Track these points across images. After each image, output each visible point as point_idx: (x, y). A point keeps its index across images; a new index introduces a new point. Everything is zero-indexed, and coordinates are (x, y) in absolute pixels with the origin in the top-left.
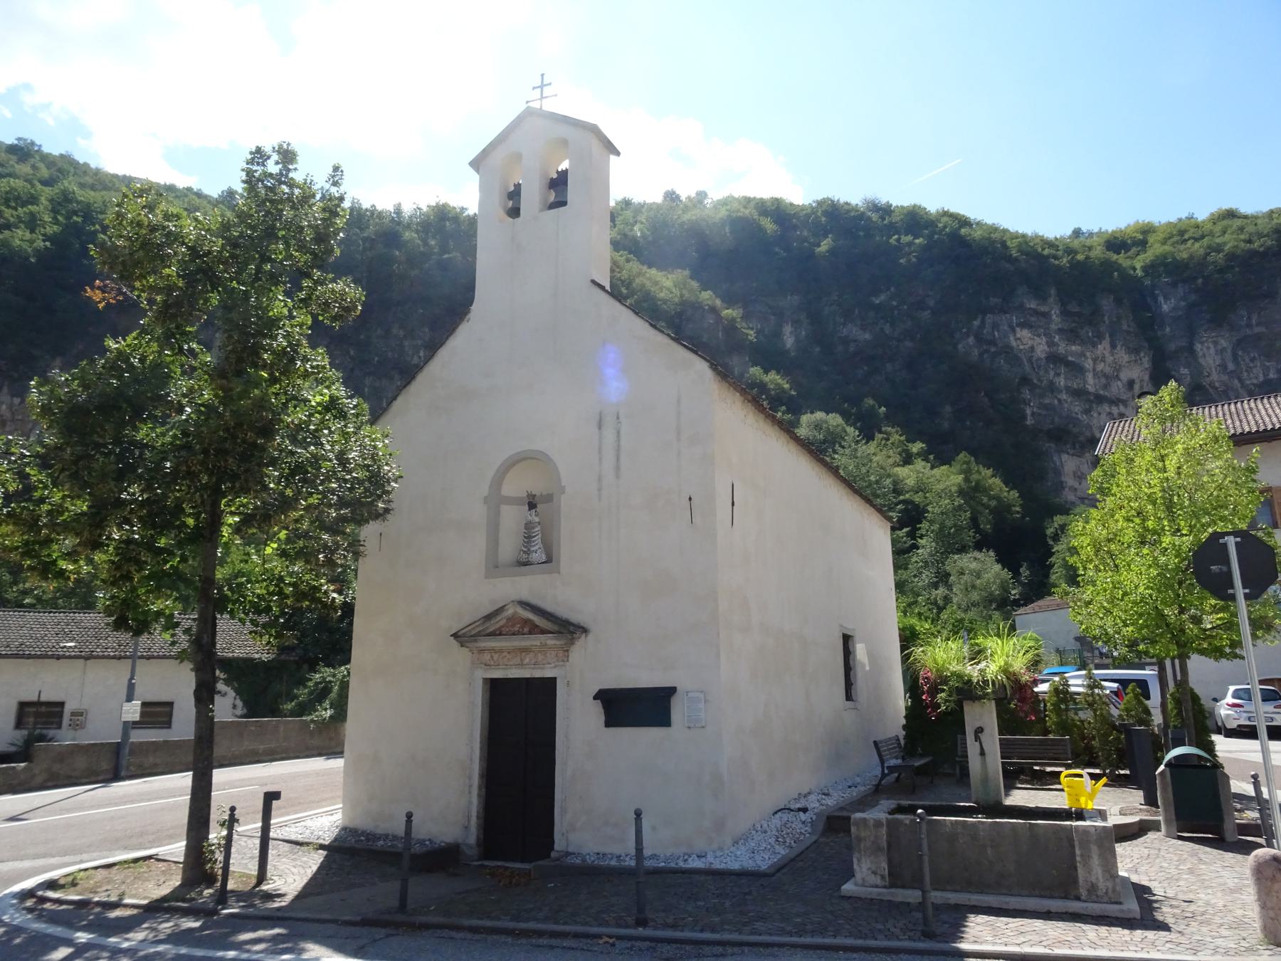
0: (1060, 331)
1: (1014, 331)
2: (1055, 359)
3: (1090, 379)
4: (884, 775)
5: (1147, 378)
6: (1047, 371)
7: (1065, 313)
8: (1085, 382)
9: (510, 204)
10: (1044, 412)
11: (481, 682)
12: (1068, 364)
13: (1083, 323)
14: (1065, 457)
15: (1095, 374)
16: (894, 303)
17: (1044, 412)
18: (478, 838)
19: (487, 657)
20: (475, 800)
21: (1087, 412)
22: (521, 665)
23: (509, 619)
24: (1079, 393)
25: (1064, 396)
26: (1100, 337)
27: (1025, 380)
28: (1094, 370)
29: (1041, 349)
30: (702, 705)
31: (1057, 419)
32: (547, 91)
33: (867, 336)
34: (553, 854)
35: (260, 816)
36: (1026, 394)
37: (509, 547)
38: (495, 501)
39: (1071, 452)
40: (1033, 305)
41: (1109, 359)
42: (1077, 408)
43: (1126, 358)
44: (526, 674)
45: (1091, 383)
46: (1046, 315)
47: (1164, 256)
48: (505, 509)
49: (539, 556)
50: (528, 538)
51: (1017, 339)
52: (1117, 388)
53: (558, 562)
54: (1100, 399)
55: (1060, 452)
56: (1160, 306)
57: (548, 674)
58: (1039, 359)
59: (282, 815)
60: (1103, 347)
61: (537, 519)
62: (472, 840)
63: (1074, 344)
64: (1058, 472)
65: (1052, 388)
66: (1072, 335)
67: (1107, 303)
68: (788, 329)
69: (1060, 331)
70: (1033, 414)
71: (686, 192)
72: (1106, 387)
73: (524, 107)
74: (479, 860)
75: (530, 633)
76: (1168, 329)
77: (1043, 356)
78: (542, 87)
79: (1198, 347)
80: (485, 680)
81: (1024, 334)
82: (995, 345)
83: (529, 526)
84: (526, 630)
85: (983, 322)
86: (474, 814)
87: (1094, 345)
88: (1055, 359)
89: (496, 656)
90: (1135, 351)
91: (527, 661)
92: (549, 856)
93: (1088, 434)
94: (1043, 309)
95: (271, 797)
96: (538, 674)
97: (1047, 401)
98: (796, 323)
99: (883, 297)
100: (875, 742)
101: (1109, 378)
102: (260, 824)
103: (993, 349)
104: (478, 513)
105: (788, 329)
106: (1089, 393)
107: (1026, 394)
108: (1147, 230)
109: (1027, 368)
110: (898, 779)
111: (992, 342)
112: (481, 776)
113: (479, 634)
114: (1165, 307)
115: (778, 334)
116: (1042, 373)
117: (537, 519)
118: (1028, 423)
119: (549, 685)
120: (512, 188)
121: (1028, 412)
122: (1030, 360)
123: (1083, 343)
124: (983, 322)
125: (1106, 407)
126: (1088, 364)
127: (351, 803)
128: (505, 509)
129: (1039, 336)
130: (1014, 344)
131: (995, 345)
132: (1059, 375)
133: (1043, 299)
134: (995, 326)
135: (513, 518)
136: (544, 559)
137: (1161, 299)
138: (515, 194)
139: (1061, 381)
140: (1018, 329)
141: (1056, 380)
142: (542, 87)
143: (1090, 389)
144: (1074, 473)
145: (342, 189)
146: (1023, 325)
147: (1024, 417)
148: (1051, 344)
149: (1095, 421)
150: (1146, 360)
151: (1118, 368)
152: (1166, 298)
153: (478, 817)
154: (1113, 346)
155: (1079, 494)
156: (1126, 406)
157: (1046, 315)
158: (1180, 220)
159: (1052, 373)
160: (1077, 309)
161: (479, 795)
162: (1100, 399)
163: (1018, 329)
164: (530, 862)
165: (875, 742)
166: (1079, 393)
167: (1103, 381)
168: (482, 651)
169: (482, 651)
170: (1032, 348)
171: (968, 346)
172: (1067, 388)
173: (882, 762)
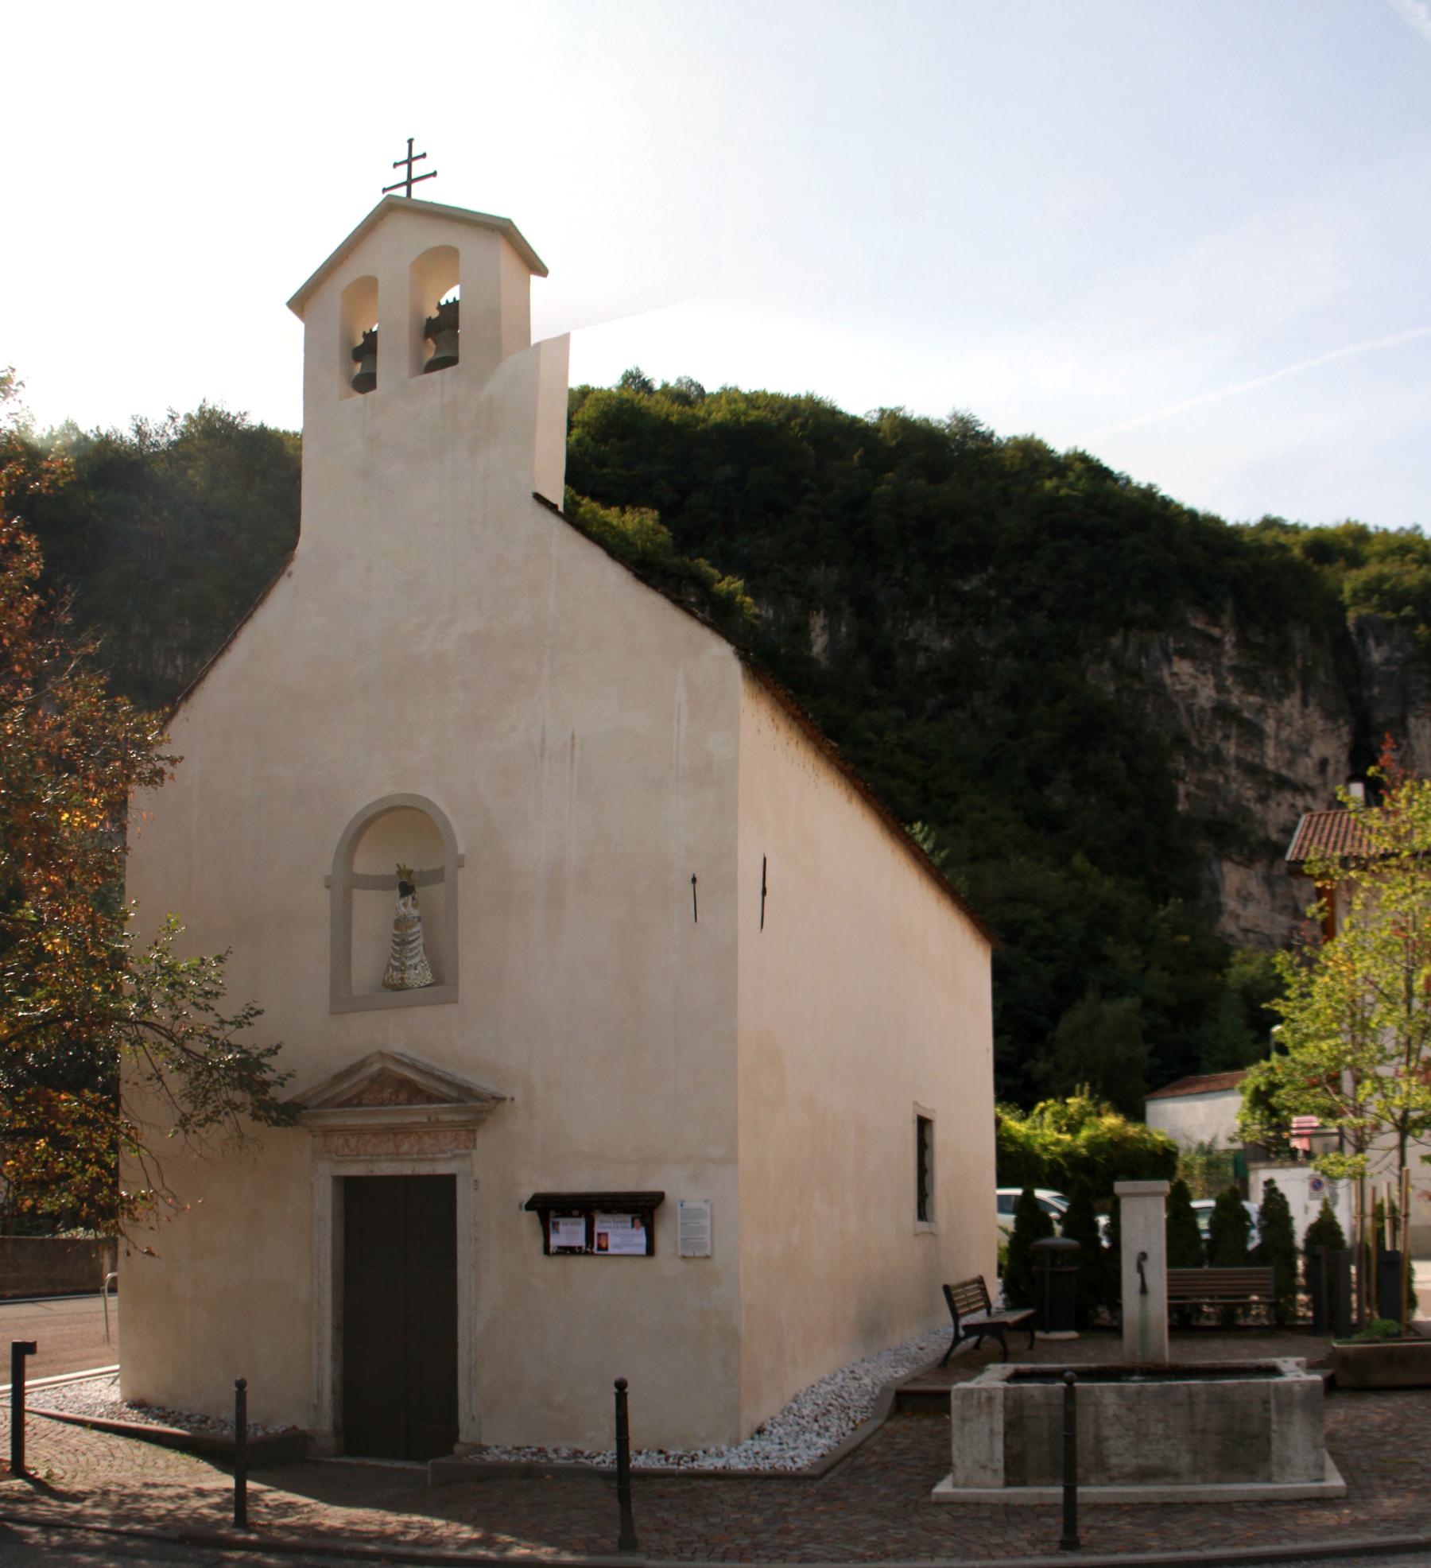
0: (1235, 670)
1: (1170, 661)
2: (1224, 713)
3: (1271, 751)
4: (957, 1339)
5: (1344, 758)
6: (1211, 731)
7: (1243, 643)
8: (1263, 754)
9: (358, 368)
10: (1202, 794)
11: (329, 1182)
12: (1243, 723)
13: (1265, 667)
14: (1227, 867)
15: (1278, 743)
16: (992, 593)
17: (1202, 794)
18: (335, 1425)
19: (338, 1141)
20: (328, 1367)
21: (1262, 799)
22: (397, 1156)
23: (372, 1079)
24: (1253, 771)
25: (1233, 771)
26: (1287, 688)
27: (1181, 741)
28: (1277, 735)
29: (1207, 695)
30: (706, 1222)
31: (1220, 807)
32: (419, 168)
33: (946, 643)
34: (457, 1448)
35: (8, 1374)
36: (1180, 763)
37: (368, 962)
38: (346, 885)
39: (1237, 858)
40: (1199, 625)
41: (1299, 729)
42: (1248, 792)
43: (1320, 724)
44: (406, 1169)
45: (1272, 756)
46: (1217, 642)
47: (1381, 579)
48: (359, 895)
49: (419, 974)
50: (402, 943)
51: (1174, 675)
52: (1305, 769)
53: (456, 984)
54: (1282, 783)
55: (1222, 855)
56: (1368, 654)
57: (442, 1169)
58: (1202, 709)
59: (36, 1377)
60: (1291, 705)
61: (416, 913)
62: (326, 1426)
63: (1252, 693)
64: (1216, 888)
65: (1218, 757)
66: (1250, 680)
67: (1299, 637)
68: (818, 622)
69: (1235, 670)
70: (1188, 795)
71: (662, 374)
72: (1290, 763)
73: (381, 197)
74: (336, 1455)
75: (410, 1102)
76: (1376, 690)
77: (1208, 705)
78: (409, 161)
79: (1412, 722)
80: (337, 1179)
81: (1183, 667)
82: (1141, 679)
83: (401, 923)
84: (402, 1097)
85: (1126, 641)
86: (327, 1386)
87: (1280, 698)
88: (1224, 713)
89: (353, 1142)
90: (1329, 715)
91: (405, 1148)
92: (451, 1452)
93: (1261, 834)
94: (1216, 632)
95: (22, 1351)
96: (424, 1169)
97: (1209, 777)
98: (833, 613)
99: (975, 581)
100: (947, 1289)
101: (1298, 750)
102: (9, 1386)
103: (1137, 686)
104: (321, 900)
105: (818, 622)
106: (1266, 771)
107: (1180, 763)
108: (1359, 535)
109: (1185, 723)
110: (977, 1346)
111: (1137, 674)
112: (336, 1329)
113: (325, 1104)
114: (1376, 656)
115: (800, 630)
116: (1204, 732)
117: (416, 913)
118: (1180, 808)
119: (450, 1181)
120: (360, 341)
121: (1182, 789)
122: (1189, 711)
123: (1264, 692)
124: (1126, 641)
125: (1288, 796)
126: (1270, 726)
127: (133, 1365)
128: (359, 895)
129: (1204, 673)
130: (1168, 681)
131: (1141, 679)
132: (1226, 737)
133: (1214, 619)
134: (1143, 649)
135: (373, 912)
136: (429, 979)
137: (1371, 642)
138: (366, 350)
139: (1231, 749)
140: (1175, 659)
141: (1223, 746)
142: (409, 161)
143: (1271, 766)
144: (1238, 891)
145: (182, 415)
146: (1184, 654)
147: (1174, 799)
148: (1220, 688)
149: (1271, 815)
150: (1345, 730)
151: (1308, 739)
152: (1378, 644)
153: (333, 1392)
154: (1305, 703)
155: (1243, 923)
156: (1314, 797)
157: (1217, 642)
158: (1401, 529)
159: (1219, 734)
160: (1260, 639)
161: (334, 1358)
162: (1282, 783)
163: (1175, 659)
164: (423, 1459)
165: (947, 1289)
166: (1253, 771)
167: (1288, 754)
168: (328, 1132)
169: (328, 1132)
170: (1194, 692)
171: (1101, 681)
172: (1239, 761)
173: (956, 1317)
